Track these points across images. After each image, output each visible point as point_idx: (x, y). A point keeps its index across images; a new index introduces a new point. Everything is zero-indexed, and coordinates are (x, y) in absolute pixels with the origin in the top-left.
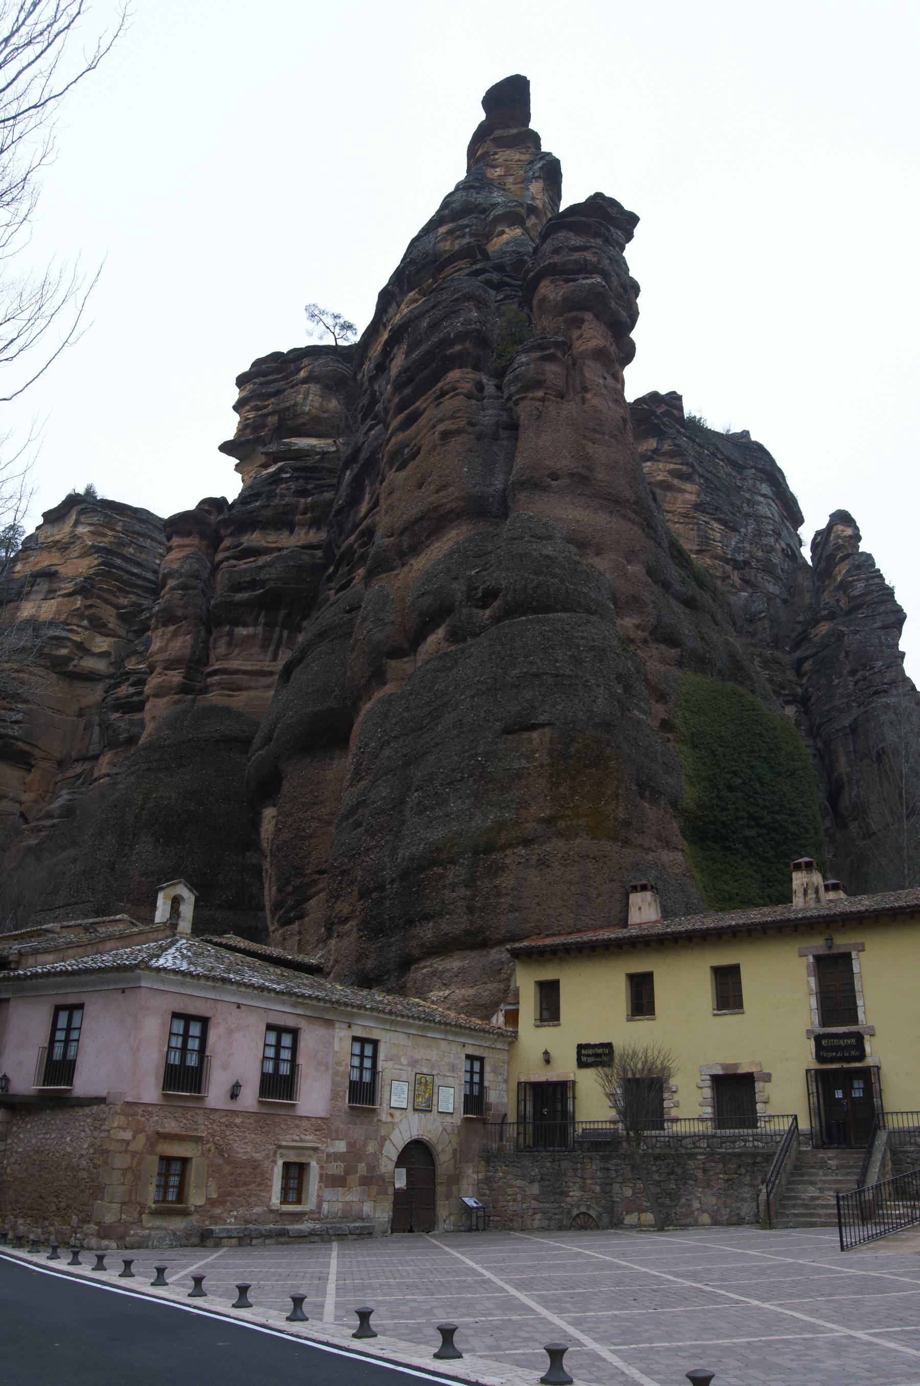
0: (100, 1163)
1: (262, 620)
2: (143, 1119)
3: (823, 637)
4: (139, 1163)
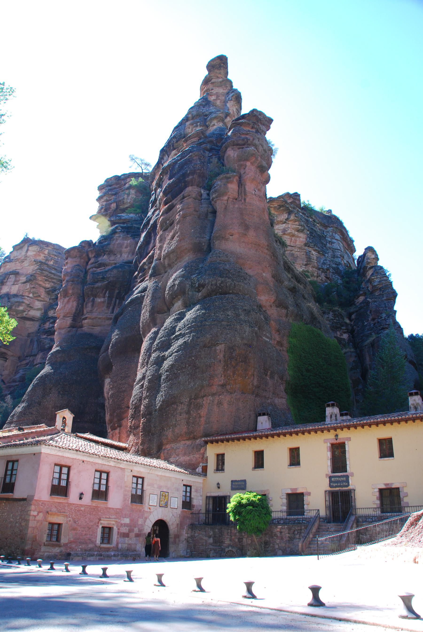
1: (107, 295)
2: (42, 507)
3: (361, 303)
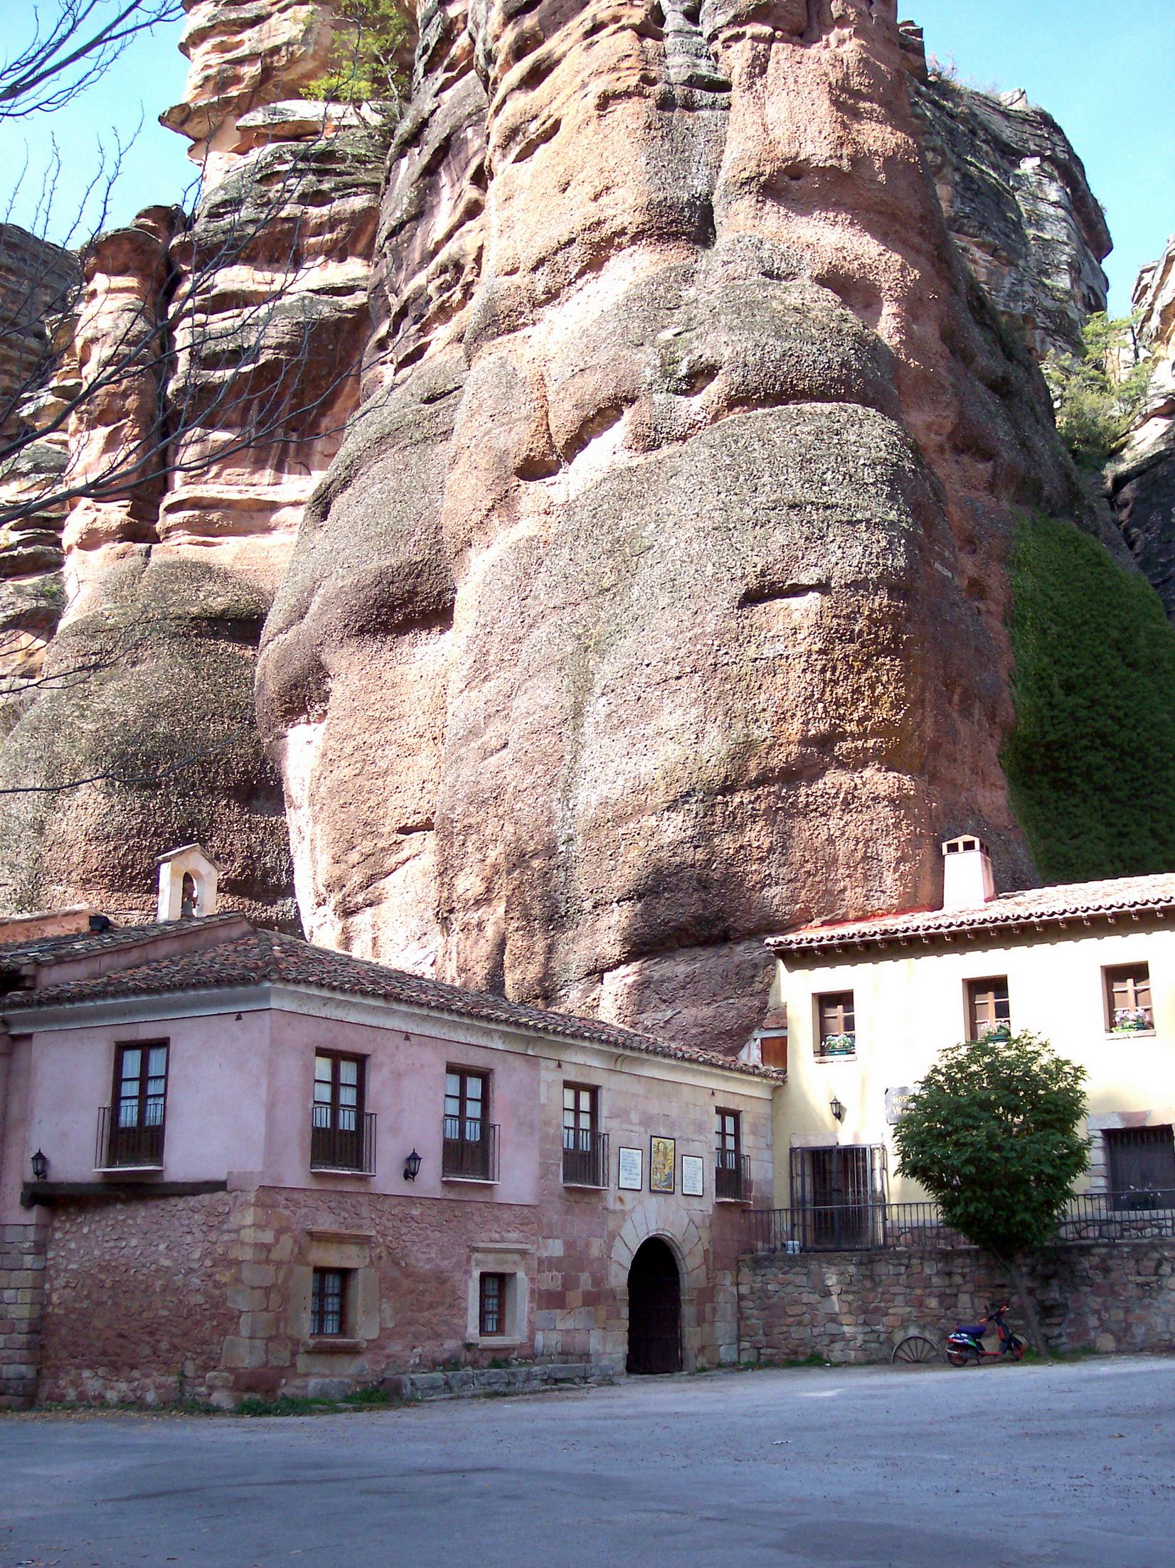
0: (224, 1280)
2: (287, 1212)
4: (286, 1280)
